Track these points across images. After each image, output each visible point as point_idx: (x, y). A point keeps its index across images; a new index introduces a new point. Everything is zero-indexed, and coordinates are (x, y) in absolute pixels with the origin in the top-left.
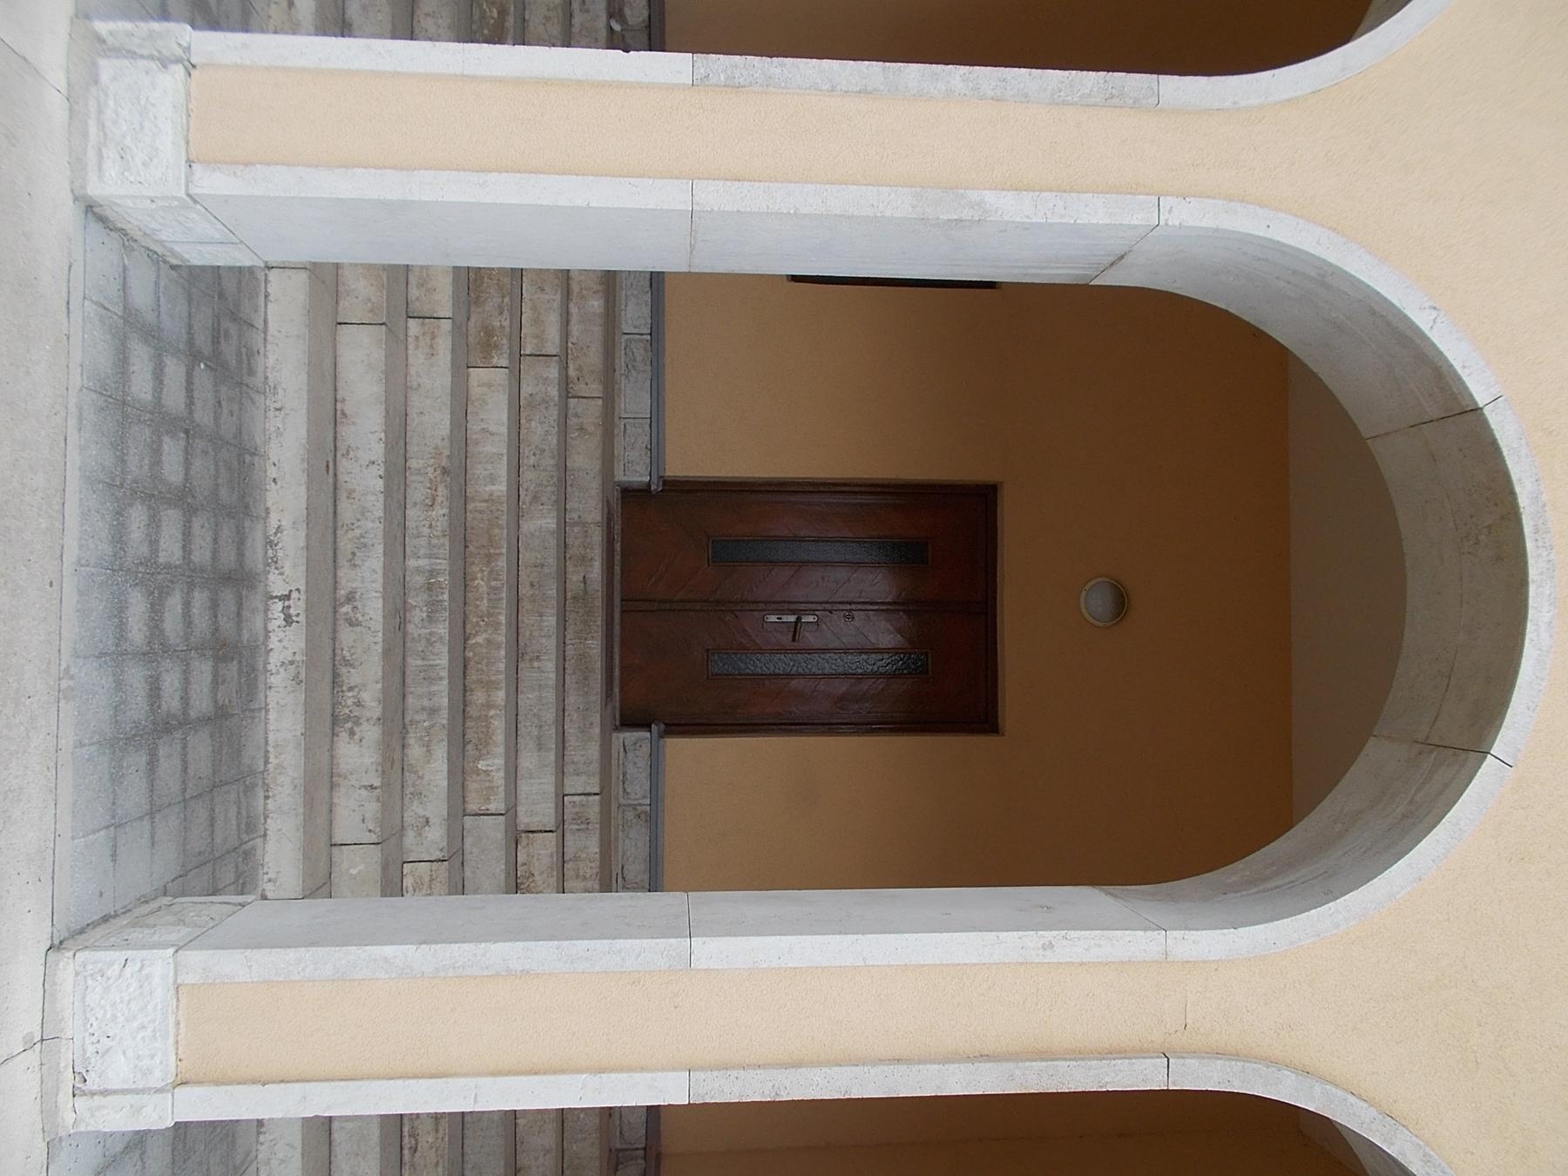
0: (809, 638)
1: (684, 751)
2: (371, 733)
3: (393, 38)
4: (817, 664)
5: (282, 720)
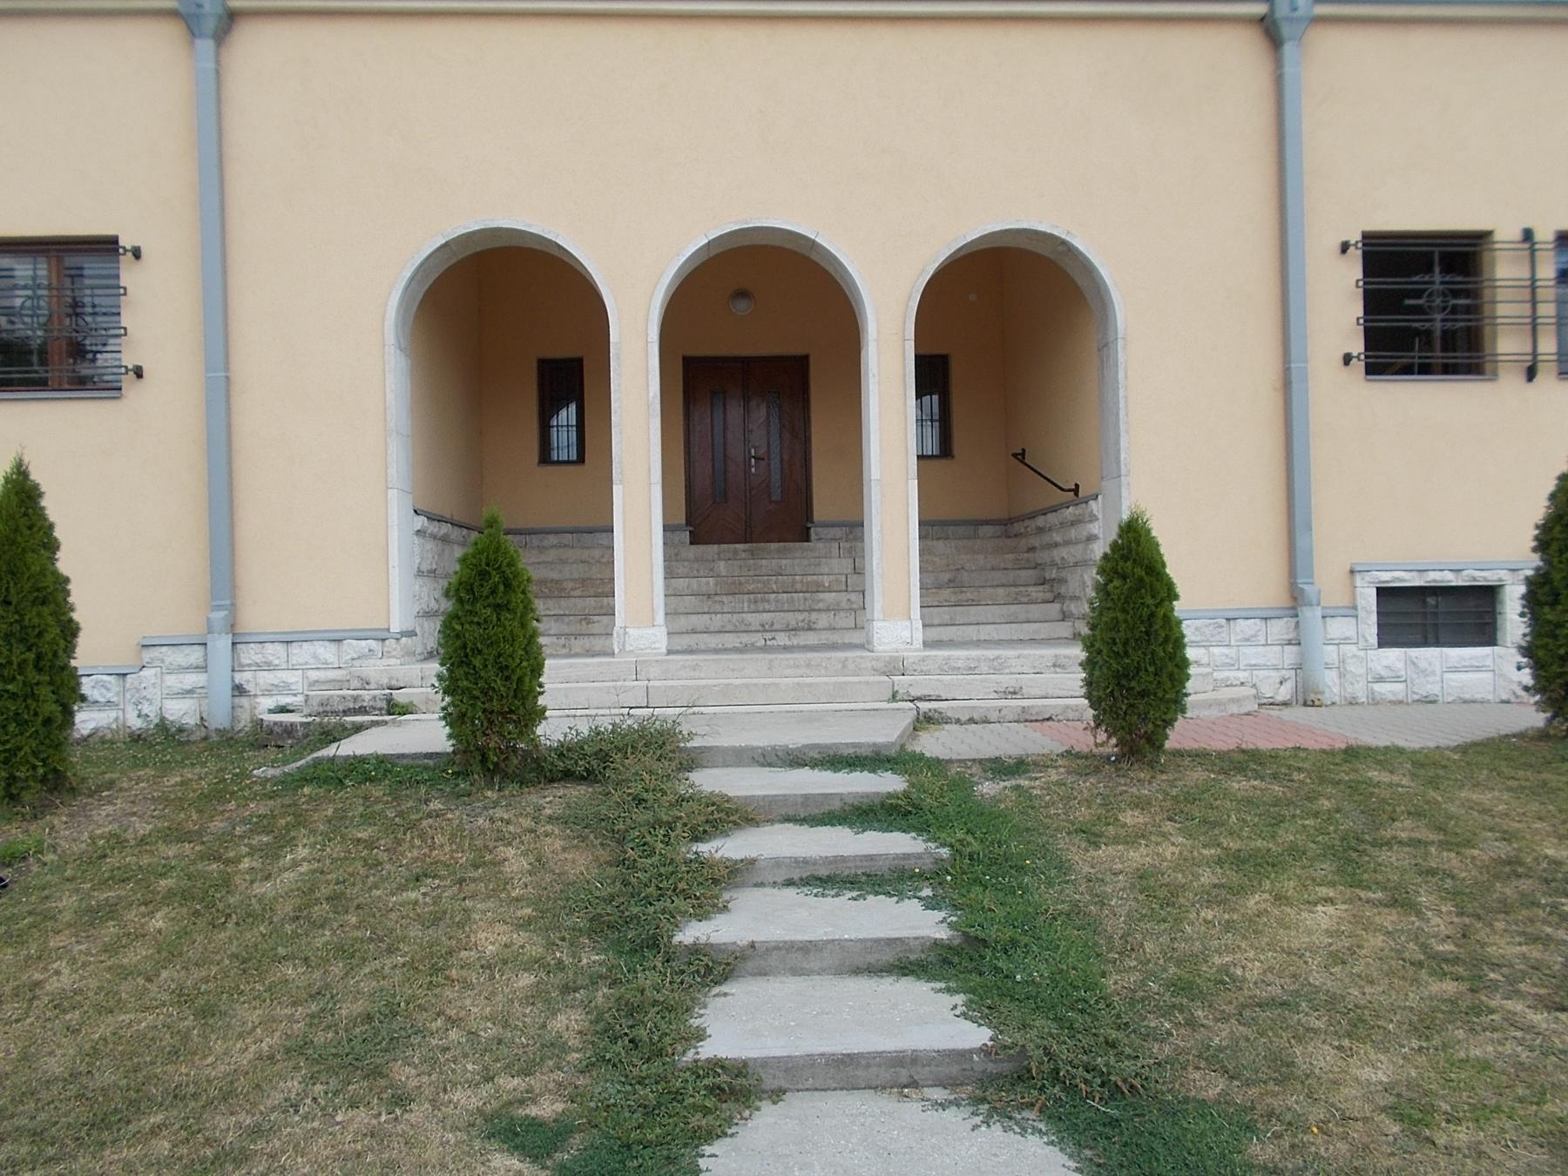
0: (762, 451)
1: (818, 515)
2: (814, 616)
3: (919, 359)
4: (775, 449)
5: (809, 680)
